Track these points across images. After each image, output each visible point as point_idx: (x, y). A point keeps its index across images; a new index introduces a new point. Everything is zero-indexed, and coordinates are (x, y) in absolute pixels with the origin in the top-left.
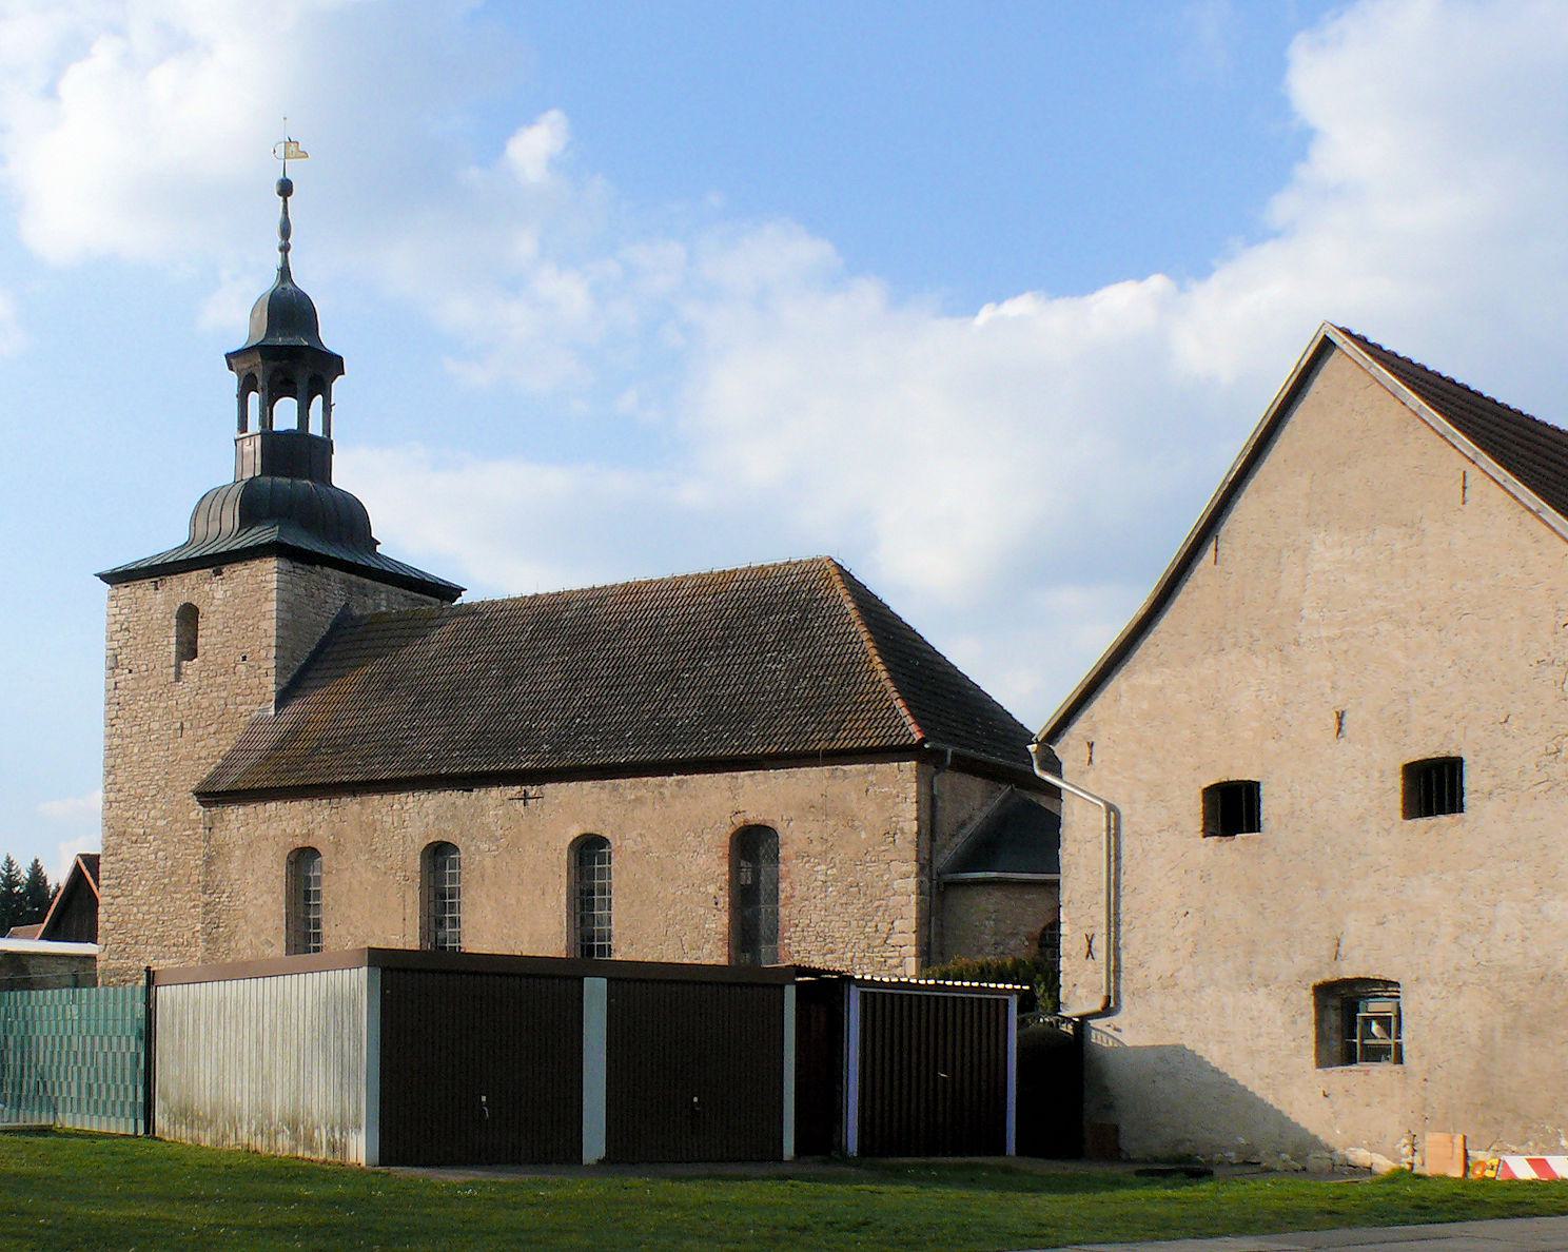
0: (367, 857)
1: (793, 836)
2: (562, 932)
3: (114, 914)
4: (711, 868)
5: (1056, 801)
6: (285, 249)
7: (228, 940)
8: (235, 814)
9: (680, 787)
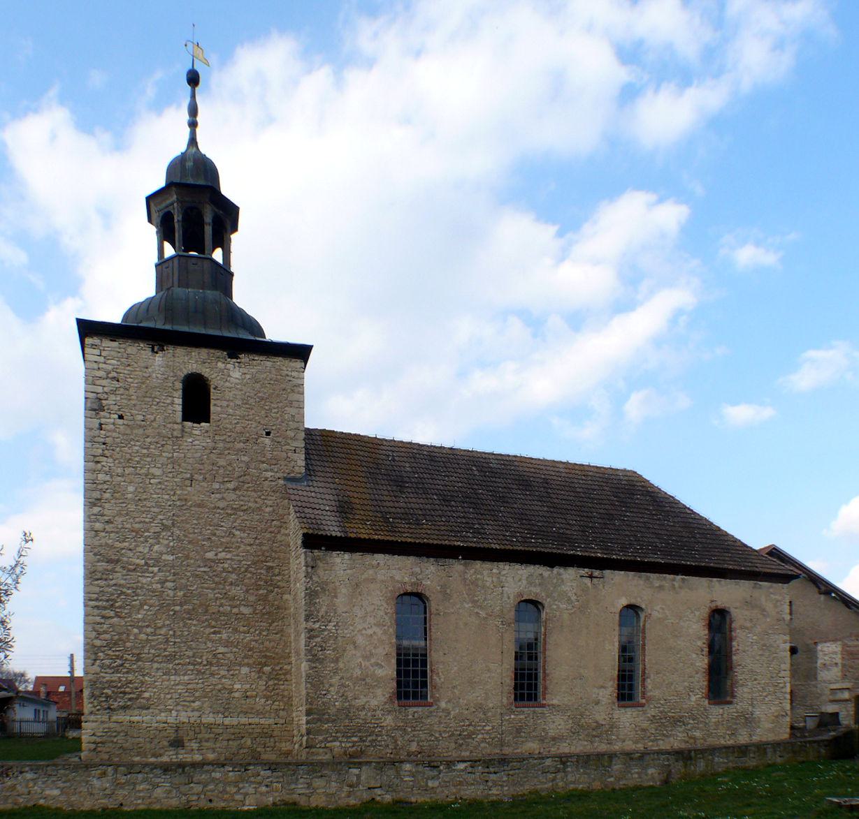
0: (470, 605)
1: (739, 616)
2: (614, 665)
3: (105, 632)
4: (697, 630)
6: (193, 125)
7: (336, 661)
8: (341, 562)
9: (683, 582)
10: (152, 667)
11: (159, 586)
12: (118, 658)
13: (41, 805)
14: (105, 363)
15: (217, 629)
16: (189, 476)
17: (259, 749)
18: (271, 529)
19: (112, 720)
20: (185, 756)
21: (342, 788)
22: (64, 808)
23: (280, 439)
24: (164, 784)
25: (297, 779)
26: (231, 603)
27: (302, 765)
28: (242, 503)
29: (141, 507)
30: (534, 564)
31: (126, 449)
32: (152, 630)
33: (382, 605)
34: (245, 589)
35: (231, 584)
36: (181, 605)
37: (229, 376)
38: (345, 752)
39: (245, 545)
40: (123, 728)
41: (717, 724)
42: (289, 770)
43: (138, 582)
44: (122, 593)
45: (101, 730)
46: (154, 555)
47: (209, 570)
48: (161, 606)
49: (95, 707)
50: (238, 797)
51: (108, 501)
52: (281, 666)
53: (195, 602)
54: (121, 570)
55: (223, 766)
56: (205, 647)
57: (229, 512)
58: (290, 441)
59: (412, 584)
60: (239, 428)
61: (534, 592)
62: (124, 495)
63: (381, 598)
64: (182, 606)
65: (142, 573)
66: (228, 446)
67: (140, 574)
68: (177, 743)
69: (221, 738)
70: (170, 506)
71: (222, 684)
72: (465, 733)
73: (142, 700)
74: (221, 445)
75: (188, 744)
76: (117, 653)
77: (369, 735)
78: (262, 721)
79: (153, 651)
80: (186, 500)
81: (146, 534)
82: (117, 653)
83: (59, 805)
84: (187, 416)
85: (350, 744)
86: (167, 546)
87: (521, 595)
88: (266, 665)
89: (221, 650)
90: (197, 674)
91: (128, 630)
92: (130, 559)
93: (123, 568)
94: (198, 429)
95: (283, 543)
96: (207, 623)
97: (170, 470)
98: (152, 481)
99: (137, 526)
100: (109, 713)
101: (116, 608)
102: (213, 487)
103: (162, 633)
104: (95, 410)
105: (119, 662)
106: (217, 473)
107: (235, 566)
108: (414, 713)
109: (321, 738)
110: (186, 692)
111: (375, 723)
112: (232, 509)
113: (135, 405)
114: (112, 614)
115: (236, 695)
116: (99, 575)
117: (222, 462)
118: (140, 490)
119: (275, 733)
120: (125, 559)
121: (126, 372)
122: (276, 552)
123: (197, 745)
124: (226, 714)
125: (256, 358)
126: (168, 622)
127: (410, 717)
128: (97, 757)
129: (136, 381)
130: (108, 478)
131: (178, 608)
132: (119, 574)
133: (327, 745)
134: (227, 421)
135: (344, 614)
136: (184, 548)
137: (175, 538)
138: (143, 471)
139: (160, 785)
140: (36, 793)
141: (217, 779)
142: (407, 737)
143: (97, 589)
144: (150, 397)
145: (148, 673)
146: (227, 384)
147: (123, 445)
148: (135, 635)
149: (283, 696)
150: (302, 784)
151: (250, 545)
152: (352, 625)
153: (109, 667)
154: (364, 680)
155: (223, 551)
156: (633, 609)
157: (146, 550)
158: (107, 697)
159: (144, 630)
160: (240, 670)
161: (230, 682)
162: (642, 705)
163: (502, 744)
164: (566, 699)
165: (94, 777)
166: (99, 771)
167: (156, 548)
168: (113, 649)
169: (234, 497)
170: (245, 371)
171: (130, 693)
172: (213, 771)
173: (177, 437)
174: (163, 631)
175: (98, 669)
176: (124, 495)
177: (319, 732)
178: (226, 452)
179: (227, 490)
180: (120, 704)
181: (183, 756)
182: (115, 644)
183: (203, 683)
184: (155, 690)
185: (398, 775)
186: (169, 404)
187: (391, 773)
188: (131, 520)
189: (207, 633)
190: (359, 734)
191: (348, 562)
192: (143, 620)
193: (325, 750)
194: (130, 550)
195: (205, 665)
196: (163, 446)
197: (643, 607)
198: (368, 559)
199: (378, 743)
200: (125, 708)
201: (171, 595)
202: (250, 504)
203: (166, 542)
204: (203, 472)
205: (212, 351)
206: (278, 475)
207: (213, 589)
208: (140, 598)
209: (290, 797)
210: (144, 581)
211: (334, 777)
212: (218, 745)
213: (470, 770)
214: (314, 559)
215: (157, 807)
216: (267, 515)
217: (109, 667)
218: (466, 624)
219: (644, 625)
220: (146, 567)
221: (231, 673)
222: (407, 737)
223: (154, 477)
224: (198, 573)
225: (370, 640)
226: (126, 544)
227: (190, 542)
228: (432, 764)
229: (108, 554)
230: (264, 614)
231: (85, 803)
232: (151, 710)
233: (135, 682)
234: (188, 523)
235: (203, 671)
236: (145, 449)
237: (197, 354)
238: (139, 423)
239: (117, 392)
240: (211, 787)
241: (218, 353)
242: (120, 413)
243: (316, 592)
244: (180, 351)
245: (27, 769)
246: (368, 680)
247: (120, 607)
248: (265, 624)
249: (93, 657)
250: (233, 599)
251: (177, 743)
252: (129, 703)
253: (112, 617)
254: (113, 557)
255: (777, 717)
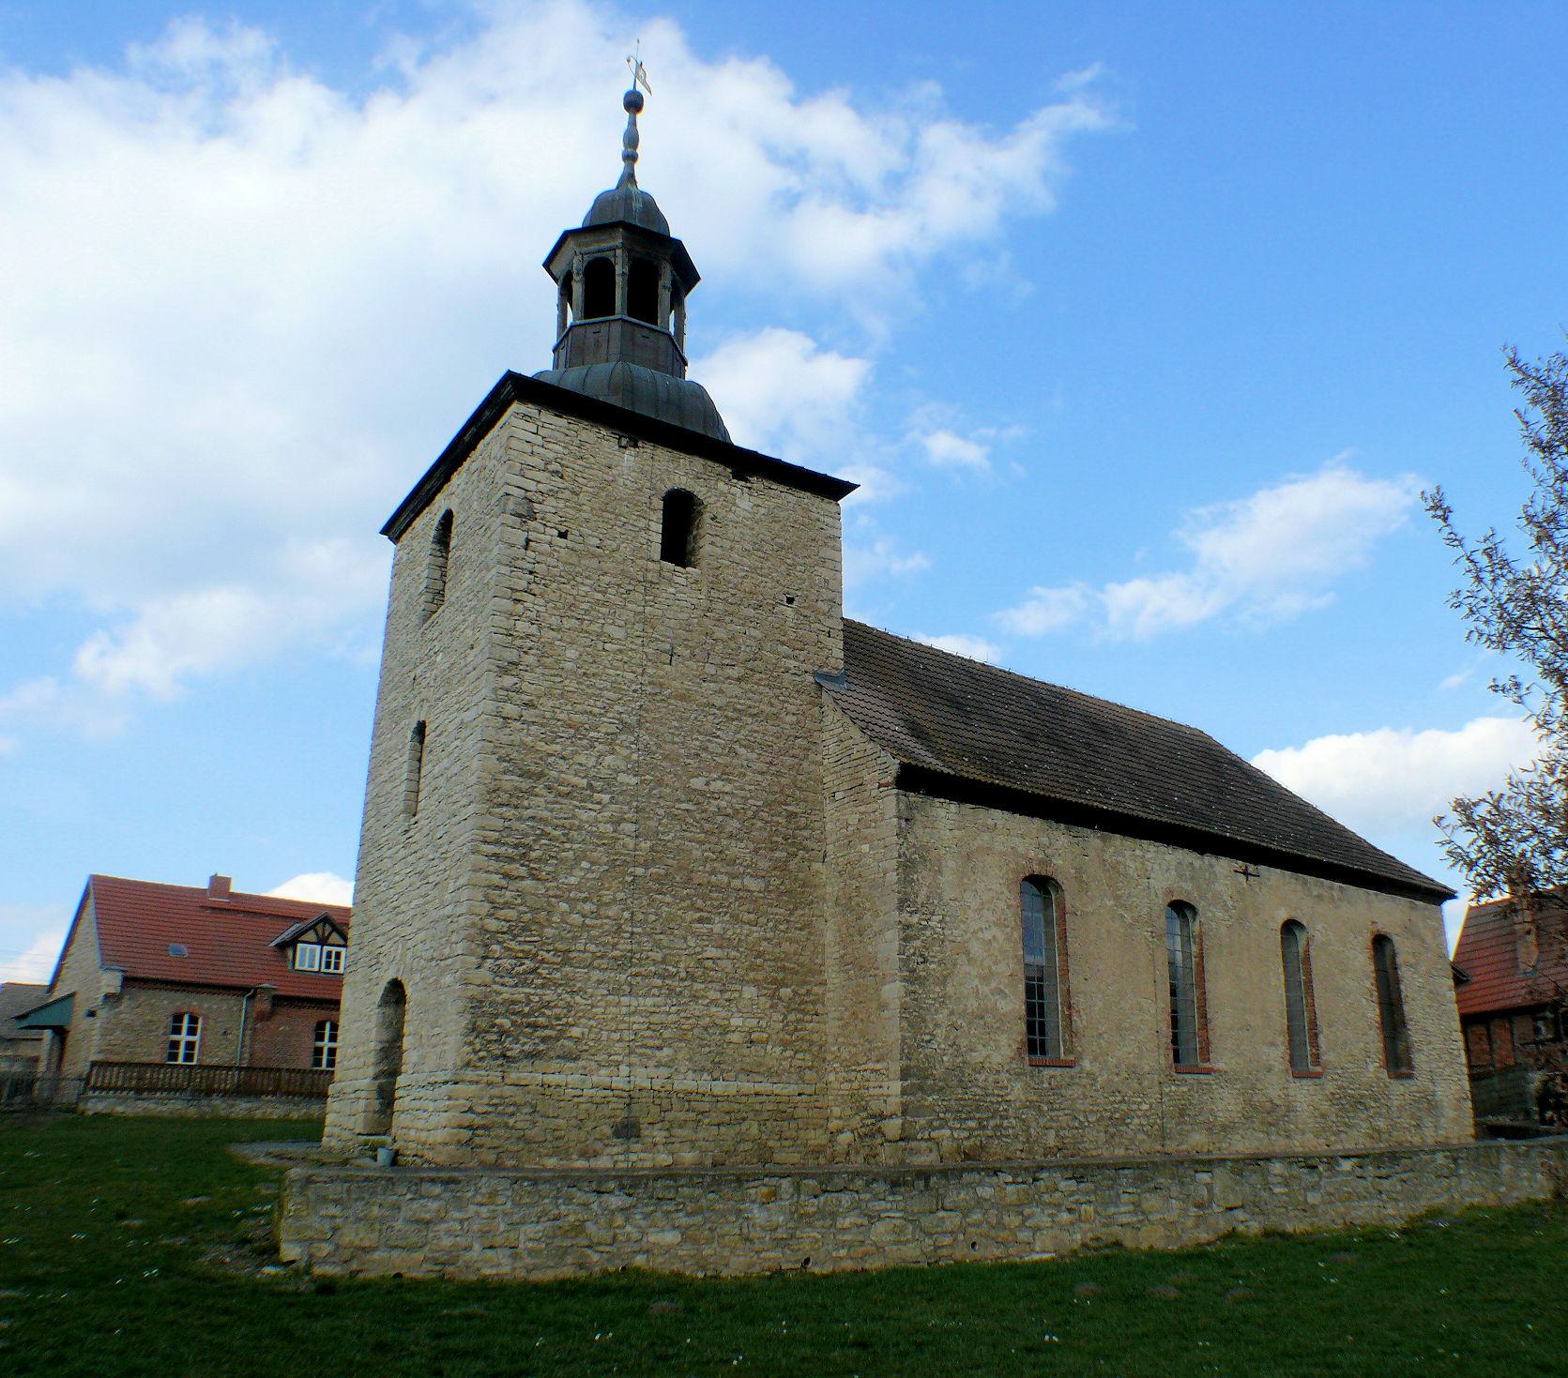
3: (507, 905)
4: (1362, 961)
5: (1460, 967)
6: (632, 140)
7: (943, 981)
8: (945, 813)
10: (589, 979)
11: (610, 828)
12: (527, 955)
13: (637, 1269)
14: (543, 446)
15: (705, 915)
16: (668, 647)
17: (770, 1143)
18: (794, 752)
19: (507, 1081)
20: (642, 1155)
21: (1186, 1210)
22: (687, 1273)
23: (807, 612)
24: (893, 1215)
25: (1118, 1196)
26: (729, 869)
27: (1123, 1168)
28: (749, 703)
29: (588, 686)
30: (1183, 846)
31: (568, 587)
32: (594, 908)
33: (1002, 893)
34: (752, 846)
35: (731, 836)
36: (646, 866)
37: (734, 504)
38: (959, 1147)
39: (754, 772)
40: (529, 1098)
41: (1400, 1108)
42: (1104, 1179)
43: (574, 817)
44: (544, 834)
45: (486, 1100)
46: (604, 773)
47: (694, 808)
48: (612, 864)
49: (476, 1052)
50: (1024, 1236)
51: (529, 668)
52: (808, 987)
53: (670, 862)
54: (544, 792)
55: (996, 1172)
56: (685, 946)
57: (730, 714)
58: (822, 618)
59: (1041, 862)
60: (747, 585)
61: (1186, 891)
62: (558, 661)
63: (1001, 881)
64: (647, 869)
65: (581, 801)
66: (731, 609)
67: (577, 804)
68: (628, 1131)
69: (707, 1121)
70: (635, 691)
71: (711, 1017)
72: (1117, 1115)
73: (566, 1043)
74: (720, 606)
75: (647, 1133)
76: (526, 947)
77: (992, 1118)
78: (777, 1089)
79: (592, 948)
80: (661, 685)
81: (592, 734)
82: (526, 947)
83: (675, 1268)
84: (666, 555)
85: (966, 1134)
86: (627, 759)
87: (1170, 892)
88: (783, 984)
89: (712, 952)
90: (668, 996)
91: (549, 904)
92: (563, 775)
93: (549, 788)
94: (682, 575)
95: (812, 775)
96: (689, 902)
97: (638, 633)
98: (608, 646)
99: (578, 718)
100: (502, 1065)
101: (530, 861)
102: (706, 670)
103: (610, 913)
104: (520, 516)
105: (529, 964)
106: (713, 649)
107: (738, 806)
108: (1051, 1077)
109: (922, 1121)
110: (648, 1028)
111: (999, 1096)
112: (735, 710)
113: (587, 521)
114: (523, 871)
115: (735, 1037)
116: (504, 798)
117: (720, 633)
118: (585, 658)
119: (798, 1110)
120: (553, 773)
121: (577, 467)
122: (800, 789)
123: (665, 1133)
124: (716, 1074)
125: (774, 487)
126: (621, 895)
127: (1046, 1085)
128: (473, 1158)
129: (592, 484)
130: (533, 630)
131: (640, 871)
132: (542, 800)
133: (933, 1134)
134: (730, 571)
135: (952, 903)
136: (656, 765)
137: (641, 746)
138: (595, 627)
139: (883, 1215)
140: (628, 1240)
141: (986, 1200)
142: (1042, 1122)
143: (499, 823)
144: (612, 513)
145: (580, 990)
146: (731, 516)
147: (563, 580)
148: (563, 914)
149: (812, 1043)
150: (1125, 1204)
151: (762, 773)
152: (964, 923)
153: (510, 973)
154: (982, 1018)
155: (719, 778)
156: (1290, 927)
157: (592, 762)
158: (501, 1033)
159: (579, 907)
160: (741, 992)
161: (724, 1014)
162: (1318, 1076)
163: (1163, 1136)
164: (1233, 1061)
165: (753, 1202)
166: (765, 1190)
167: (609, 759)
168: (519, 939)
169: (738, 691)
170: (759, 502)
171: (545, 1027)
172: (980, 1183)
173: (652, 582)
174: (613, 911)
175: (488, 977)
176: (558, 661)
177: (920, 1110)
178: (728, 619)
179: (728, 678)
180: (526, 1048)
181: (641, 1158)
182: (523, 929)
183: (678, 1013)
184: (592, 1022)
185: (1267, 1186)
186: (641, 529)
187: (1255, 1179)
188: (569, 707)
189: (688, 919)
190: (978, 1116)
191: (956, 817)
192: (578, 888)
193: (929, 1144)
194: (563, 758)
195: (682, 980)
196: (628, 592)
197: (1305, 923)
198: (981, 816)
199: (1003, 1132)
200: (532, 1056)
201: (631, 846)
202: (763, 707)
203: (625, 752)
204: (690, 644)
205: (710, 463)
206: (804, 667)
207: (701, 843)
208: (575, 846)
209: (1108, 1230)
210: (584, 816)
211: (1175, 1190)
212: (701, 1135)
213: (1359, 1171)
214: (910, 807)
215: (874, 1264)
216: (788, 727)
217: (510, 973)
218: (1109, 932)
219: (1307, 952)
220: (588, 792)
221: (727, 996)
222: (1042, 1122)
223: (611, 639)
224: (676, 812)
225: (989, 950)
226: (558, 748)
227: (665, 757)
228: (1309, 1162)
229: (522, 760)
230: (782, 893)
231: (733, 1259)
232: (581, 1063)
233: (556, 1006)
234: (663, 725)
235: (678, 989)
236: (599, 592)
237: (687, 463)
238: (592, 549)
239: (560, 495)
240: (976, 1217)
241: (720, 468)
242: (563, 529)
243: (912, 861)
244: (663, 454)
245: (612, 1185)
246: (988, 1019)
247: (539, 860)
248: (782, 911)
249: (481, 952)
250: (733, 862)
251: (628, 1131)
252: (542, 1047)
253: (522, 878)
254: (533, 768)
255: (1458, 1100)
